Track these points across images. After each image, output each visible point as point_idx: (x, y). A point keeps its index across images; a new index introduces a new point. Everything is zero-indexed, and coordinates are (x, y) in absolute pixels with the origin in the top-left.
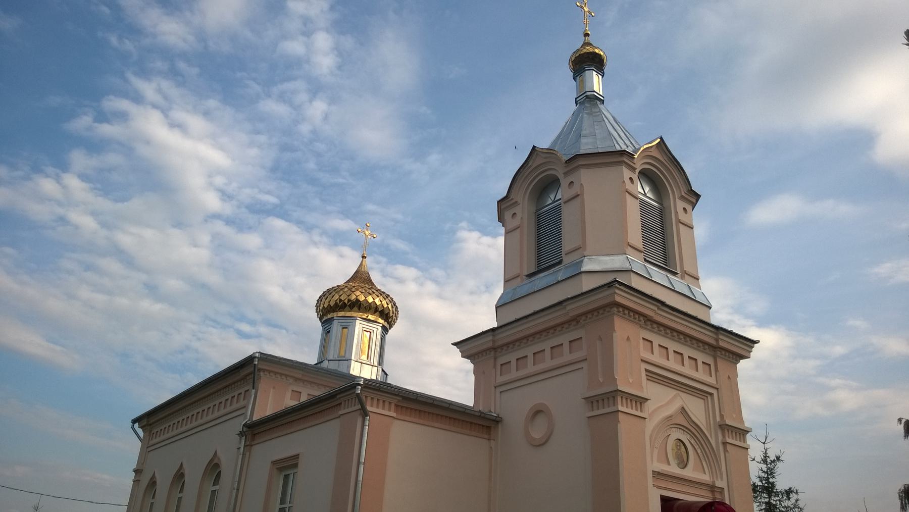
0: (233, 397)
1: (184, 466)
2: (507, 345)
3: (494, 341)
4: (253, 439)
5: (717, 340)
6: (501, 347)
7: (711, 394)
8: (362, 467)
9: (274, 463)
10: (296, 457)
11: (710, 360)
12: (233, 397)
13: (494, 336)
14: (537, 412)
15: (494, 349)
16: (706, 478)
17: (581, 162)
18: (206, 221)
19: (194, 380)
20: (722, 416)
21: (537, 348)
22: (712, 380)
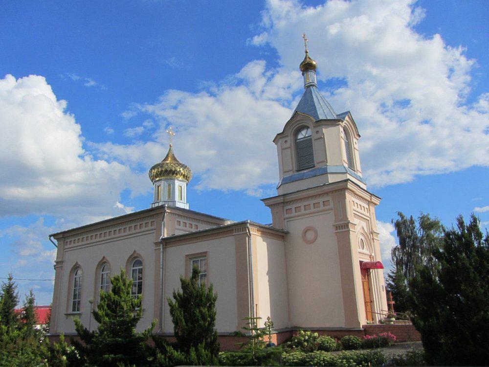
0: (92, 236)
1: (404, 214)
2: (291, 201)
3: (284, 200)
4: (166, 245)
5: (371, 199)
6: (287, 202)
7: (368, 220)
8: (161, 266)
9: (187, 256)
10: (206, 252)
11: (366, 206)
12: (92, 236)
13: (284, 198)
14: (307, 230)
15: (284, 203)
16: (368, 252)
17: (323, 123)
18: (463, 113)
19: (75, 226)
20: (372, 229)
21: (315, 201)
22: (368, 215)
